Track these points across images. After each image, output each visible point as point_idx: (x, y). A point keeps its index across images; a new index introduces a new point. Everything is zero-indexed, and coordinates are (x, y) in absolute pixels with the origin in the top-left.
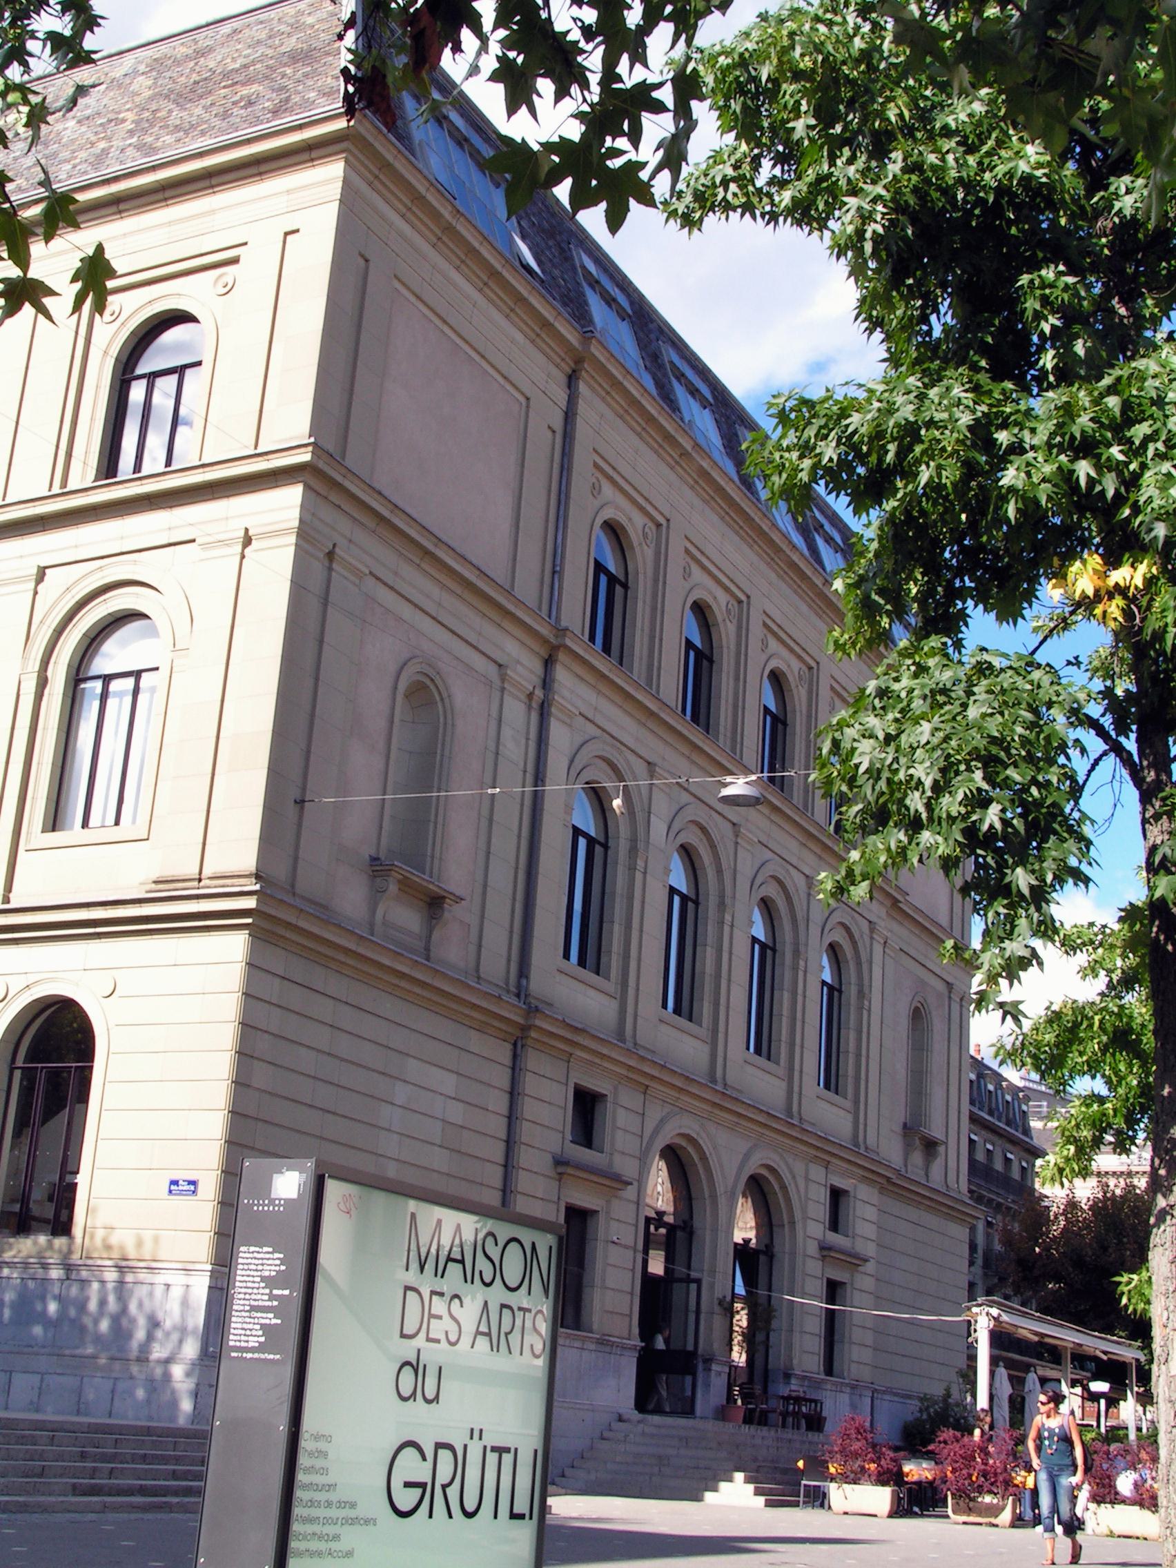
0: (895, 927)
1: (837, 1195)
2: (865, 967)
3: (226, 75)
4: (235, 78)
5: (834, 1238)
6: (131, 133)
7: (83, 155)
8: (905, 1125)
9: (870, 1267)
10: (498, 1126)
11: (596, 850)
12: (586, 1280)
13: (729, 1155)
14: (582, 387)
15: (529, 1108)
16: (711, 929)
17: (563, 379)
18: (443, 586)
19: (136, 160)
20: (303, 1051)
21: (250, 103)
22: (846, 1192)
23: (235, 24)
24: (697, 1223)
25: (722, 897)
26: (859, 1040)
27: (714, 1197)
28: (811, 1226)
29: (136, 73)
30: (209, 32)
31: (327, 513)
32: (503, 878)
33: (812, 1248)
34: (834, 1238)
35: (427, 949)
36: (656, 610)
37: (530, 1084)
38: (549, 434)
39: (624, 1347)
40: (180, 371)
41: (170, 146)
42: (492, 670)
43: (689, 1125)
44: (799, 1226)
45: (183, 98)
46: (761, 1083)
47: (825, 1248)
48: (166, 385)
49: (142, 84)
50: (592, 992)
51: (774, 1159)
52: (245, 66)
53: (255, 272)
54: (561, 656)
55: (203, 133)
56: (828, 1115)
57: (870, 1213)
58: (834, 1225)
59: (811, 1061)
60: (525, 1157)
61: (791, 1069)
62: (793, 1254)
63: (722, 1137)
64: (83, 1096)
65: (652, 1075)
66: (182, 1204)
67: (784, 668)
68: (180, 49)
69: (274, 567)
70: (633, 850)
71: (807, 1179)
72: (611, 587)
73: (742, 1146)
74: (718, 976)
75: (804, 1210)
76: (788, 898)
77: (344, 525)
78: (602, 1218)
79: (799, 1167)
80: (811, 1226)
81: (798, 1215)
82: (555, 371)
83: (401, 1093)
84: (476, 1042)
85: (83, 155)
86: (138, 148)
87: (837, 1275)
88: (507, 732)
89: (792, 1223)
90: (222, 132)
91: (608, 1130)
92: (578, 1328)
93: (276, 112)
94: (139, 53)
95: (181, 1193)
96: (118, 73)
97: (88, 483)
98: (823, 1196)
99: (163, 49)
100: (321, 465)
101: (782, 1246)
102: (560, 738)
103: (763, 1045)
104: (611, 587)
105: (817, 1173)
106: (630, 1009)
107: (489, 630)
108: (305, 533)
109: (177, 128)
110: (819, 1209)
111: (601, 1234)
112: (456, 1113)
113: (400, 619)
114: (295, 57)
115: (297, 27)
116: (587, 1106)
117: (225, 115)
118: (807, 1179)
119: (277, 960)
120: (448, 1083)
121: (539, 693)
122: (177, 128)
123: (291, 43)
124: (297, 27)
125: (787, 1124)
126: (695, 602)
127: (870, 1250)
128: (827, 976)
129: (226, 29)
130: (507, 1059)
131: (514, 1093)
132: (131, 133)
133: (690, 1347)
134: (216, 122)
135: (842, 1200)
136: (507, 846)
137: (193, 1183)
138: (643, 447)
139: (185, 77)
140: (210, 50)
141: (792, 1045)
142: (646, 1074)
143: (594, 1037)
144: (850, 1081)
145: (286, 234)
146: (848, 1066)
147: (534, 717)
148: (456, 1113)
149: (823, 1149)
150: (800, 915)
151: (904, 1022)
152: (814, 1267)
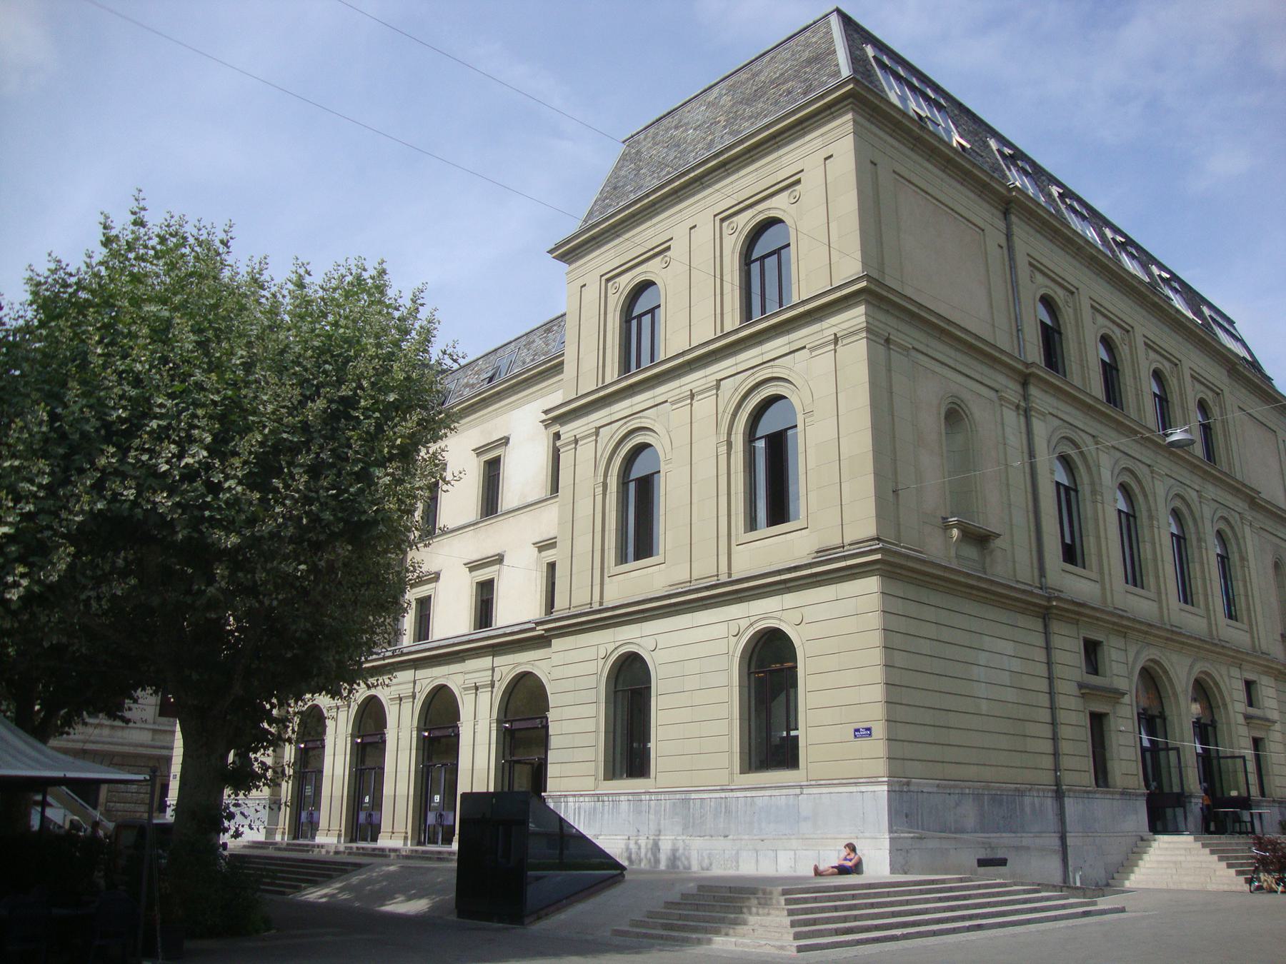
0: (1254, 513)
1: (1249, 685)
2: (1241, 541)
3: (772, 82)
4: (776, 83)
5: (1251, 711)
6: (725, 127)
7: (700, 146)
8: (1282, 635)
9: (1277, 727)
10: (1042, 670)
11: (1068, 495)
12: (1108, 755)
13: (1181, 672)
14: (1014, 219)
15: (1058, 656)
16: (1146, 532)
17: (1001, 216)
18: (957, 350)
19: (729, 140)
20: (922, 641)
21: (790, 93)
22: (1254, 682)
23: (771, 54)
24: (1167, 713)
25: (1149, 510)
26: (1245, 586)
27: (1175, 694)
28: (1237, 705)
29: (721, 96)
30: (758, 63)
31: (881, 316)
32: (1021, 519)
33: (1241, 719)
34: (1251, 711)
35: (984, 568)
36: (1081, 344)
37: (1057, 641)
38: (999, 250)
39: (1137, 795)
40: (777, 252)
41: (747, 128)
42: (992, 395)
43: (1153, 653)
44: (1230, 707)
45: (748, 101)
46: (1193, 622)
47: (1248, 717)
48: (771, 262)
49: (726, 100)
50: (1083, 580)
51: (1207, 667)
52: (782, 74)
53: (811, 185)
54: (1032, 380)
55: (765, 116)
56: (1234, 634)
57: (1271, 692)
58: (1250, 704)
59: (1218, 603)
60: (1061, 686)
61: (1208, 609)
62: (1229, 724)
63: (1175, 658)
64: (795, 684)
65: (1125, 626)
66: (864, 744)
67: (1160, 366)
68: (743, 76)
69: (857, 353)
70: (1094, 492)
71: (1230, 677)
72: (1051, 337)
73: (1188, 661)
74: (1155, 560)
75: (1231, 695)
76: (1188, 506)
77: (892, 322)
78: (1112, 718)
79: (1224, 670)
80: (1237, 705)
81: (1228, 699)
82: (995, 211)
83: (983, 658)
84: (1022, 620)
85: (700, 146)
86: (730, 133)
87: (1258, 734)
88: (1008, 430)
89: (1225, 705)
90: (776, 112)
91: (1107, 663)
92: (1107, 786)
93: (805, 94)
94: (722, 85)
95: (862, 736)
96: (711, 98)
97: (737, 325)
98: (1241, 686)
99: (734, 78)
100: (873, 287)
101: (1221, 717)
102: (1039, 428)
103: (1186, 596)
104: (1051, 337)
105: (1235, 672)
106: (1108, 586)
107: (986, 370)
108: (870, 331)
109: (750, 117)
110: (1241, 695)
111: (1113, 727)
112: (1016, 665)
113: (933, 372)
114: (809, 62)
115: (807, 45)
116: (1092, 649)
117: (776, 103)
118: (1230, 677)
119: (898, 588)
120: (1008, 647)
121: (1022, 404)
122: (750, 117)
123: (806, 55)
124: (807, 45)
125: (1210, 646)
126: (445, 686)
127: (1275, 715)
128: (1219, 551)
129: (767, 58)
130: (1040, 628)
131: (1048, 648)
132: (725, 127)
133: (1176, 789)
134: (772, 108)
135: (1253, 687)
136: (1020, 498)
137: (869, 729)
138: (1054, 247)
139: (749, 89)
140: (761, 71)
141: (1206, 596)
142: (1123, 626)
143: (1093, 608)
144: (1245, 613)
145: (826, 159)
146: (1241, 602)
147: (1022, 419)
148: (1016, 665)
149: (1236, 657)
150: (1197, 515)
151: (1271, 572)
152: (1243, 731)
